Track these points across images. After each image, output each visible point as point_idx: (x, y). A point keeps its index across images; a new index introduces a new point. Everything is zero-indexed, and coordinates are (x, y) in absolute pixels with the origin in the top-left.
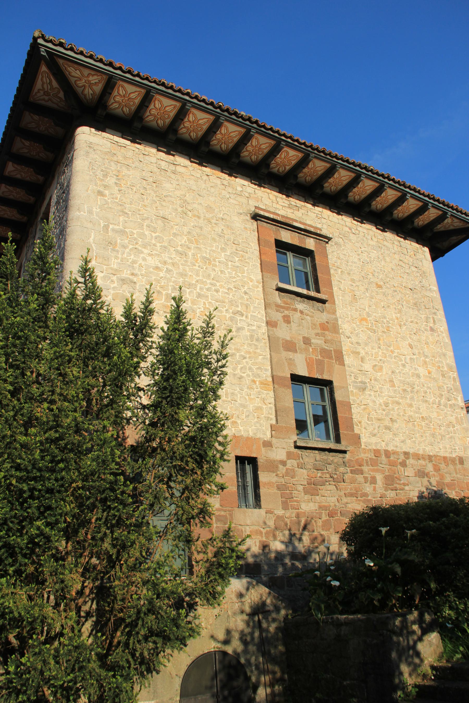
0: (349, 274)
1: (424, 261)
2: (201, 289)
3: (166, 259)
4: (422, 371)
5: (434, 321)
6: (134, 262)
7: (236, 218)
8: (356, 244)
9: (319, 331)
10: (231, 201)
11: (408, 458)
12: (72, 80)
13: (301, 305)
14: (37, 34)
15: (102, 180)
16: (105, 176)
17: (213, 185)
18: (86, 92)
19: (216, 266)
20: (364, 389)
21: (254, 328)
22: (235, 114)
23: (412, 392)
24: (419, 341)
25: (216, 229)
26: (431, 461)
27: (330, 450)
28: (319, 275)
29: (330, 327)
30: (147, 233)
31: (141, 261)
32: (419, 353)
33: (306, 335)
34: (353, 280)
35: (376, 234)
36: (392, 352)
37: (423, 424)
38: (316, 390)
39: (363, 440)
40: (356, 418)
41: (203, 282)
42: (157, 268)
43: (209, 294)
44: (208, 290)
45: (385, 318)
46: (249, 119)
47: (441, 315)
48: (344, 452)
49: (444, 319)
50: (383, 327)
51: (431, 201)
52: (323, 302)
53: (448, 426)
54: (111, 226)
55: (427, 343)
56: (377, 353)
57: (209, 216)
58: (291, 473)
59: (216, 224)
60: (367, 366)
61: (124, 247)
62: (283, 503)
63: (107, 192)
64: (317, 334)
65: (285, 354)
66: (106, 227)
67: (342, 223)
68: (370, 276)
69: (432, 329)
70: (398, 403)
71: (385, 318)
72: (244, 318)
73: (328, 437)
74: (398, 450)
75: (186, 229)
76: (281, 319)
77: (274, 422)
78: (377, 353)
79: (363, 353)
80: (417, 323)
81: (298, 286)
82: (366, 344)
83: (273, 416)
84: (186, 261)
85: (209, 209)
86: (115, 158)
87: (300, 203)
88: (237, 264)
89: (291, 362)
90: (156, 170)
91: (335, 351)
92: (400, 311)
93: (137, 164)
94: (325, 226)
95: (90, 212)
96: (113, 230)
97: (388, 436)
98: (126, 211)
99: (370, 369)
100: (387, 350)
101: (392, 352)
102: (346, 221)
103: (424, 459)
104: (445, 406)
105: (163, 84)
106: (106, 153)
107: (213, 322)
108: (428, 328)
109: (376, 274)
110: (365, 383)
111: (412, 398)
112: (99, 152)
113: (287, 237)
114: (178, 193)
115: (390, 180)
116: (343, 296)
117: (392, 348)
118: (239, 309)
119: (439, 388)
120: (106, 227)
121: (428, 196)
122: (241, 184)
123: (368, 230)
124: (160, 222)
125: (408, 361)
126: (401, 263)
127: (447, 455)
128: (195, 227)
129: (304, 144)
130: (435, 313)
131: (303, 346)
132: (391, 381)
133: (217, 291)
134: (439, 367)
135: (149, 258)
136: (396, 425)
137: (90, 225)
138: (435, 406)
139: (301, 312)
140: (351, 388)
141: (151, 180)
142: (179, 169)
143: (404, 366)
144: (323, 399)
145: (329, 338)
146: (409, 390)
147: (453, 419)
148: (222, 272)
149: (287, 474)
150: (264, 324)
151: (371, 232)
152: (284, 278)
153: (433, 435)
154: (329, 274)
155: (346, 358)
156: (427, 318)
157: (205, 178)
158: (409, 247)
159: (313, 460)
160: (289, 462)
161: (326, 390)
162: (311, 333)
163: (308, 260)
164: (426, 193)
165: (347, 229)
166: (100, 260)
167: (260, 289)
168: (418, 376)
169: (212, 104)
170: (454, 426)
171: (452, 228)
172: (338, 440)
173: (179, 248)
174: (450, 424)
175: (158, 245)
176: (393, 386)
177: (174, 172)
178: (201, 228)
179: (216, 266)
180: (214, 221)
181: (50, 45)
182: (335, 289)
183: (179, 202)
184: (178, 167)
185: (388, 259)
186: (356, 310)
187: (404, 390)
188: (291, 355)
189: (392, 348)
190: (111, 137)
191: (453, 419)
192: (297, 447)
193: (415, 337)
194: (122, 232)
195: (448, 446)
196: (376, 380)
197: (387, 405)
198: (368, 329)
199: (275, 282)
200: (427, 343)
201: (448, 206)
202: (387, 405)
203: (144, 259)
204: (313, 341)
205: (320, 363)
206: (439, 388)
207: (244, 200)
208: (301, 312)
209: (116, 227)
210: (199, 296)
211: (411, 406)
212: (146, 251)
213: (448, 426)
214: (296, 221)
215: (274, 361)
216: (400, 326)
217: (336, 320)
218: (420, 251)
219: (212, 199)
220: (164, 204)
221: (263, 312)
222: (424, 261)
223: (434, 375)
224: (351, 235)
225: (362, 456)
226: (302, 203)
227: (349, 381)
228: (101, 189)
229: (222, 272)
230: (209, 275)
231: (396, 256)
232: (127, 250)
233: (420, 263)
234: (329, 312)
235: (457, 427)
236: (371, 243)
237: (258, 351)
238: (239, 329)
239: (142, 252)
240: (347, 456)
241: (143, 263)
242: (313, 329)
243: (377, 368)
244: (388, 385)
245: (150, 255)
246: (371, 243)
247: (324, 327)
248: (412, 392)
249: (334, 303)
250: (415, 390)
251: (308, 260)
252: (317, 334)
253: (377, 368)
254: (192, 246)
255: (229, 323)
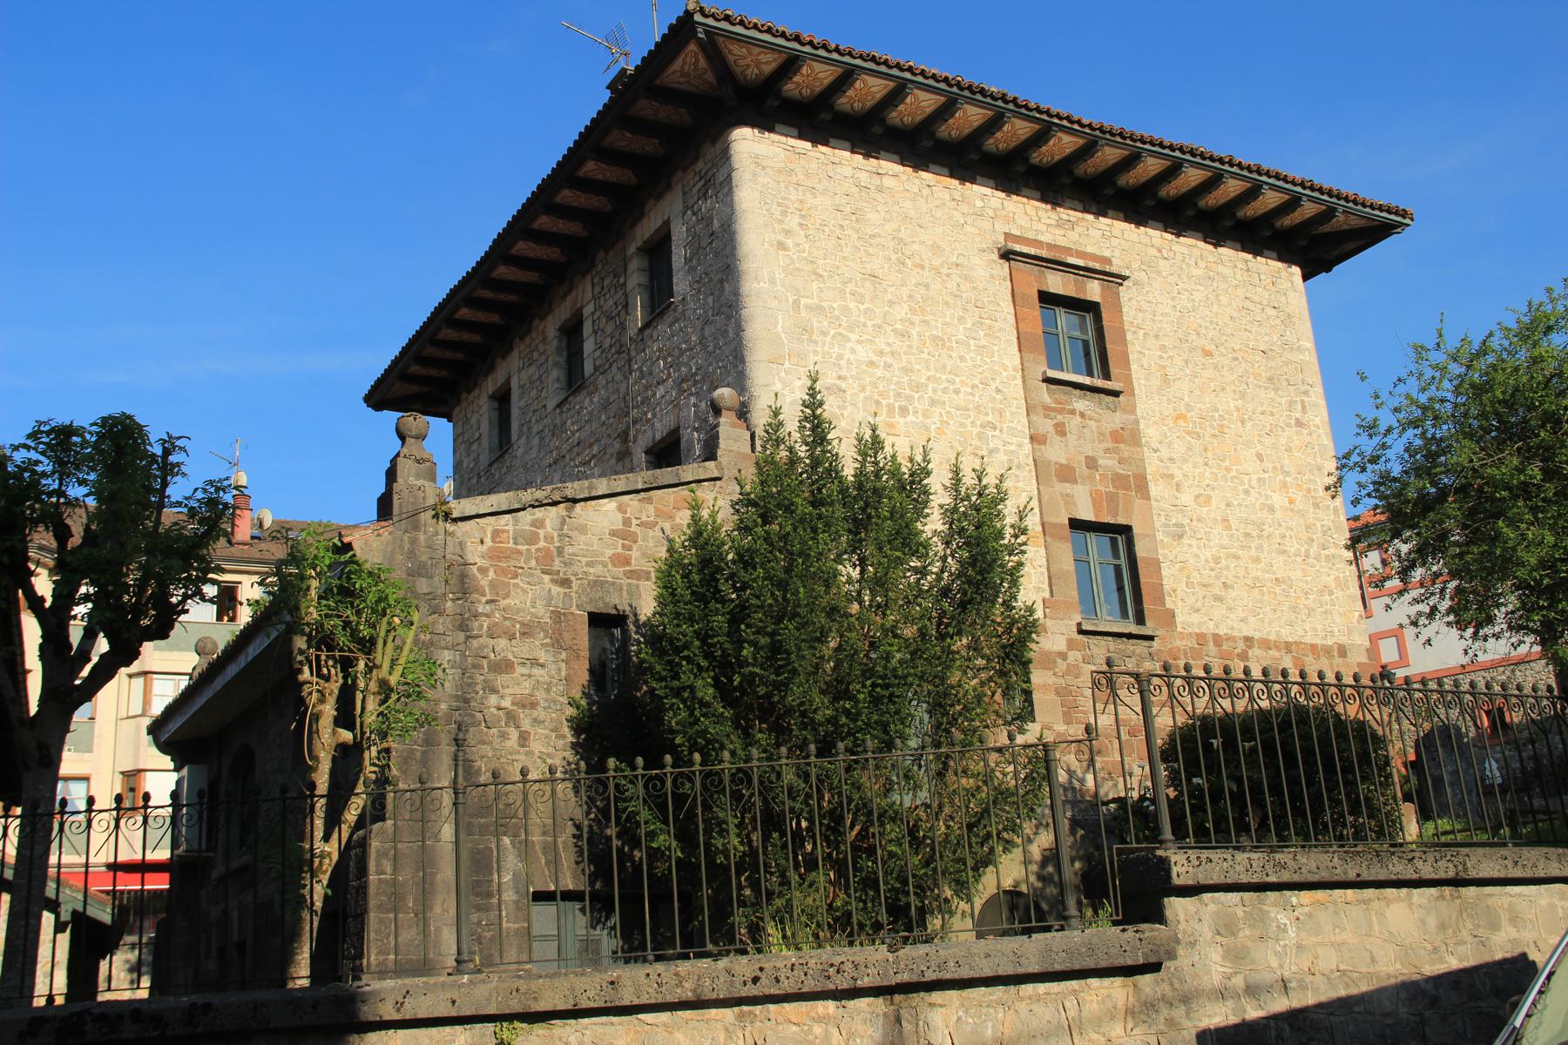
0: (1157, 336)
1: (1291, 294)
2: (934, 391)
3: (883, 346)
4: (1278, 500)
5: (1304, 408)
6: (840, 357)
7: (976, 261)
8: (1170, 279)
9: (1110, 445)
10: (968, 229)
11: (1250, 647)
12: (731, 58)
13: (1082, 403)
14: (691, 7)
15: (780, 222)
16: (784, 213)
17: (938, 203)
18: (749, 72)
19: (951, 349)
20: (1181, 537)
21: (1013, 448)
22: (982, 92)
23: (1259, 537)
24: (1275, 446)
25: (949, 285)
26: (1289, 651)
27: (1130, 636)
28: (1109, 346)
29: (1127, 437)
30: (851, 305)
31: (848, 355)
32: (1274, 468)
33: (1090, 453)
34: (1163, 348)
35: (1205, 254)
36: (1228, 470)
37: (1278, 590)
38: (1105, 540)
39: (1179, 619)
40: (1168, 583)
41: (937, 380)
42: (872, 364)
43: (946, 398)
44: (944, 391)
45: (1216, 410)
46: (1003, 98)
47: (1317, 395)
48: (1151, 638)
49: (1323, 402)
50: (1212, 426)
51: (1307, 192)
52: (1116, 394)
53: (1321, 592)
54: (803, 301)
55: (1289, 450)
56: (1202, 475)
57: (937, 262)
58: (1073, 671)
59: (948, 275)
60: (1186, 498)
61: (824, 333)
62: (1064, 714)
63: (789, 242)
64: (1107, 450)
65: (1060, 487)
66: (796, 303)
67: (1146, 240)
68: (1193, 336)
69: (1299, 423)
70: (1237, 557)
71: (1216, 410)
72: (997, 433)
73: (1124, 615)
74: (1235, 633)
75: (905, 291)
76: (1052, 430)
77: (1047, 594)
78: (1202, 475)
79: (1178, 475)
80: (1272, 414)
81: (1075, 372)
82: (1185, 460)
83: (1046, 586)
84: (910, 347)
85: (936, 248)
86: (794, 179)
87: (1075, 215)
88: (983, 342)
89: (1069, 499)
90: (854, 190)
91: (1135, 476)
92: (1243, 396)
93: (825, 182)
94: (1117, 253)
95: (772, 281)
96: (806, 307)
97: (1219, 611)
98: (820, 271)
99: (1191, 503)
100: (1219, 467)
101: (1228, 470)
102: (1153, 238)
103: (1277, 648)
104: (1318, 558)
105: (873, 59)
106: (780, 171)
107: (1005, 485)
108: (1293, 422)
109: (1203, 331)
110: (1182, 526)
111: (1260, 548)
112: (769, 171)
113: (1057, 283)
114: (889, 227)
115: (1232, 165)
116: (1147, 379)
117: (1227, 463)
118: (990, 418)
119: (1308, 527)
120: (796, 303)
121: (1302, 185)
122: (983, 196)
123: (1191, 249)
124: (868, 284)
125: (1254, 483)
126: (1247, 304)
127: (1318, 642)
128: (918, 285)
129: (1090, 126)
130: (1306, 393)
131: (1086, 471)
132: (1226, 520)
133: (957, 392)
134: (1309, 491)
135: (858, 348)
136: (1232, 594)
137: (774, 304)
138: (1299, 559)
139: (1082, 415)
140: (1160, 536)
141: (848, 210)
142: (888, 182)
143: (1247, 492)
144: (1116, 555)
145: (1126, 454)
146: (1254, 534)
147: (1330, 581)
148: (961, 358)
149: (1068, 672)
150: (1027, 441)
151: (1196, 252)
152: (1055, 363)
153: (1294, 609)
154: (1124, 342)
155: (1151, 486)
156: (1291, 403)
157: (926, 191)
158: (1263, 268)
159: (1104, 651)
160: (1070, 653)
161: (1120, 540)
162: (1096, 449)
163: (1089, 318)
164: (1298, 178)
165: (1154, 252)
166: (795, 360)
167: (1019, 381)
168: (1271, 509)
169: (946, 80)
170: (1331, 593)
171: (1345, 227)
172: (1140, 619)
173: (898, 326)
174: (1325, 589)
175: (869, 323)
176: (1229, 528)
177: (880, 190)
178: (927, 286)
179: (951, 349)
180: (945, 271)
181: (710, 22)
182: (1134, 367)
183: (891, 244)
184: (885, 179)
185: (1224, 299)
186: (1169, 401)
187: (1247, 535)
188: (1067, 488)
189: (1227, 463)
190: (783, 139)
191: (1330, 581)
192: (1081, 632)
193: (1267, 441)
194: (818, 309)
195: (1319, 627)
196: (1199, 520)
197: (1217, 560)
198: (1188, 433)
199: (1041, 368)
200: (1289, 450)
201: (1339, 197)
202: (1217, 560)
203: (853, 351)
204: (1101, 462)
205: (1112, 498)
206: (1308, 527)
207: (986, 224)
208: (1082, 415)
209: (809, 301)
210: (933, 402)
211: (1257, 560)
212: (853, 337)
213: (1321, 592)
214: (1068, 251)
215: (1045, 498)
216: (1243, 422)
217: (1137, 422)
218: (1284, 274)
219: (939, 230)
220: (871, 250)
221: (1025, 420)
222: (1291, 294)
223: (1299, 505)
224: (1162, 262)
225: (1178, 643)
226: (1079, 215)
227: (1157, 525)
228: (781, 237)
229: (961, 358)
230: (944, 367)
231: (1240, 291)
232: (828, 338)
233: (1283, 299)
234: (1124, 411)
235: (1338, 594)
236: (1195, 272)
237: (1020, 484)
238: (992, 451)
239: (849, 340)
240: (1155, 644)
241: (852, 358)
242: (1101, 441)
243: (1202, 500)
244: (1219, 528)
245: (859, 342)
246: (1195, 272)
247: (1117, 437)
248: (1259, 537)
249: (1133, 394)
250: (1265, 534)
251: (1089, 318)
252: (1107, 450)
253: (1201, 499)
254: (917, 319)
255: (976, 442)
